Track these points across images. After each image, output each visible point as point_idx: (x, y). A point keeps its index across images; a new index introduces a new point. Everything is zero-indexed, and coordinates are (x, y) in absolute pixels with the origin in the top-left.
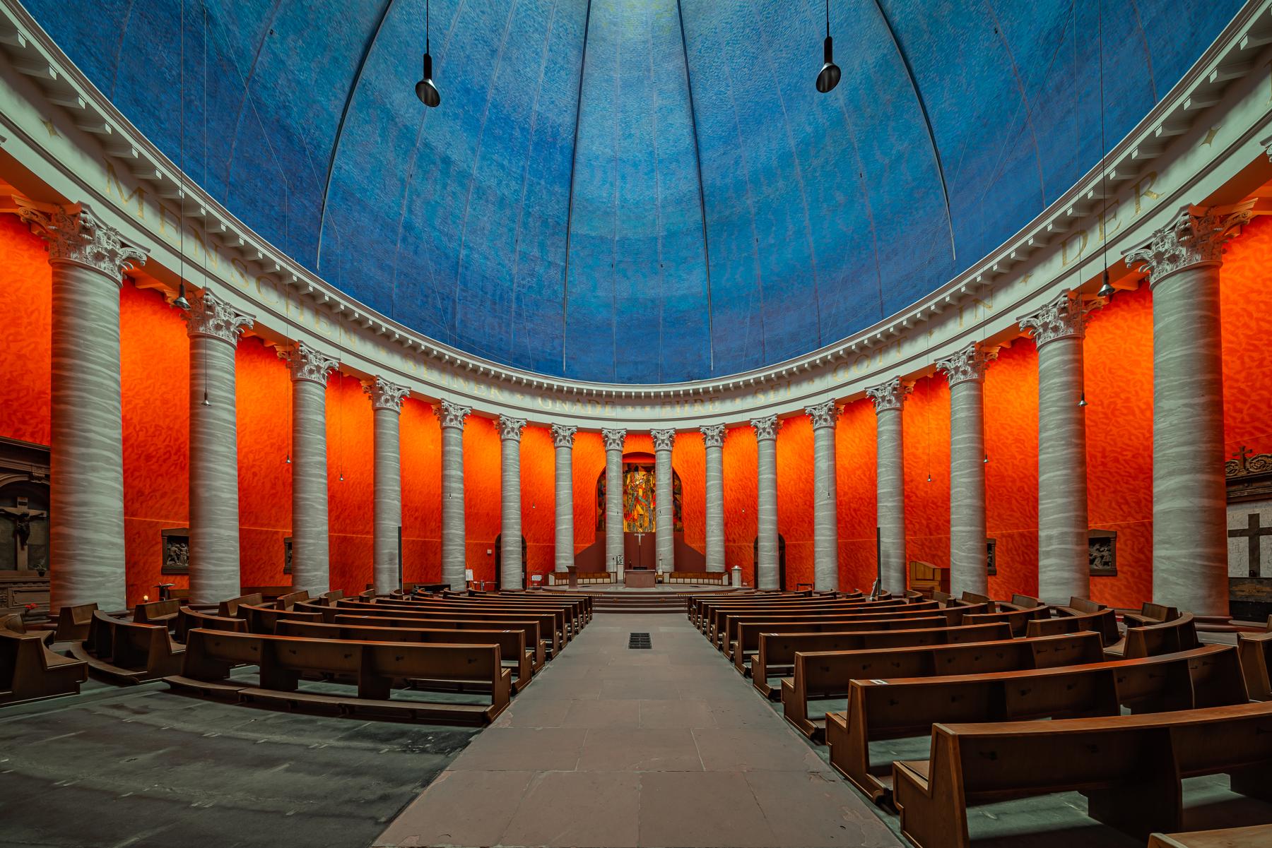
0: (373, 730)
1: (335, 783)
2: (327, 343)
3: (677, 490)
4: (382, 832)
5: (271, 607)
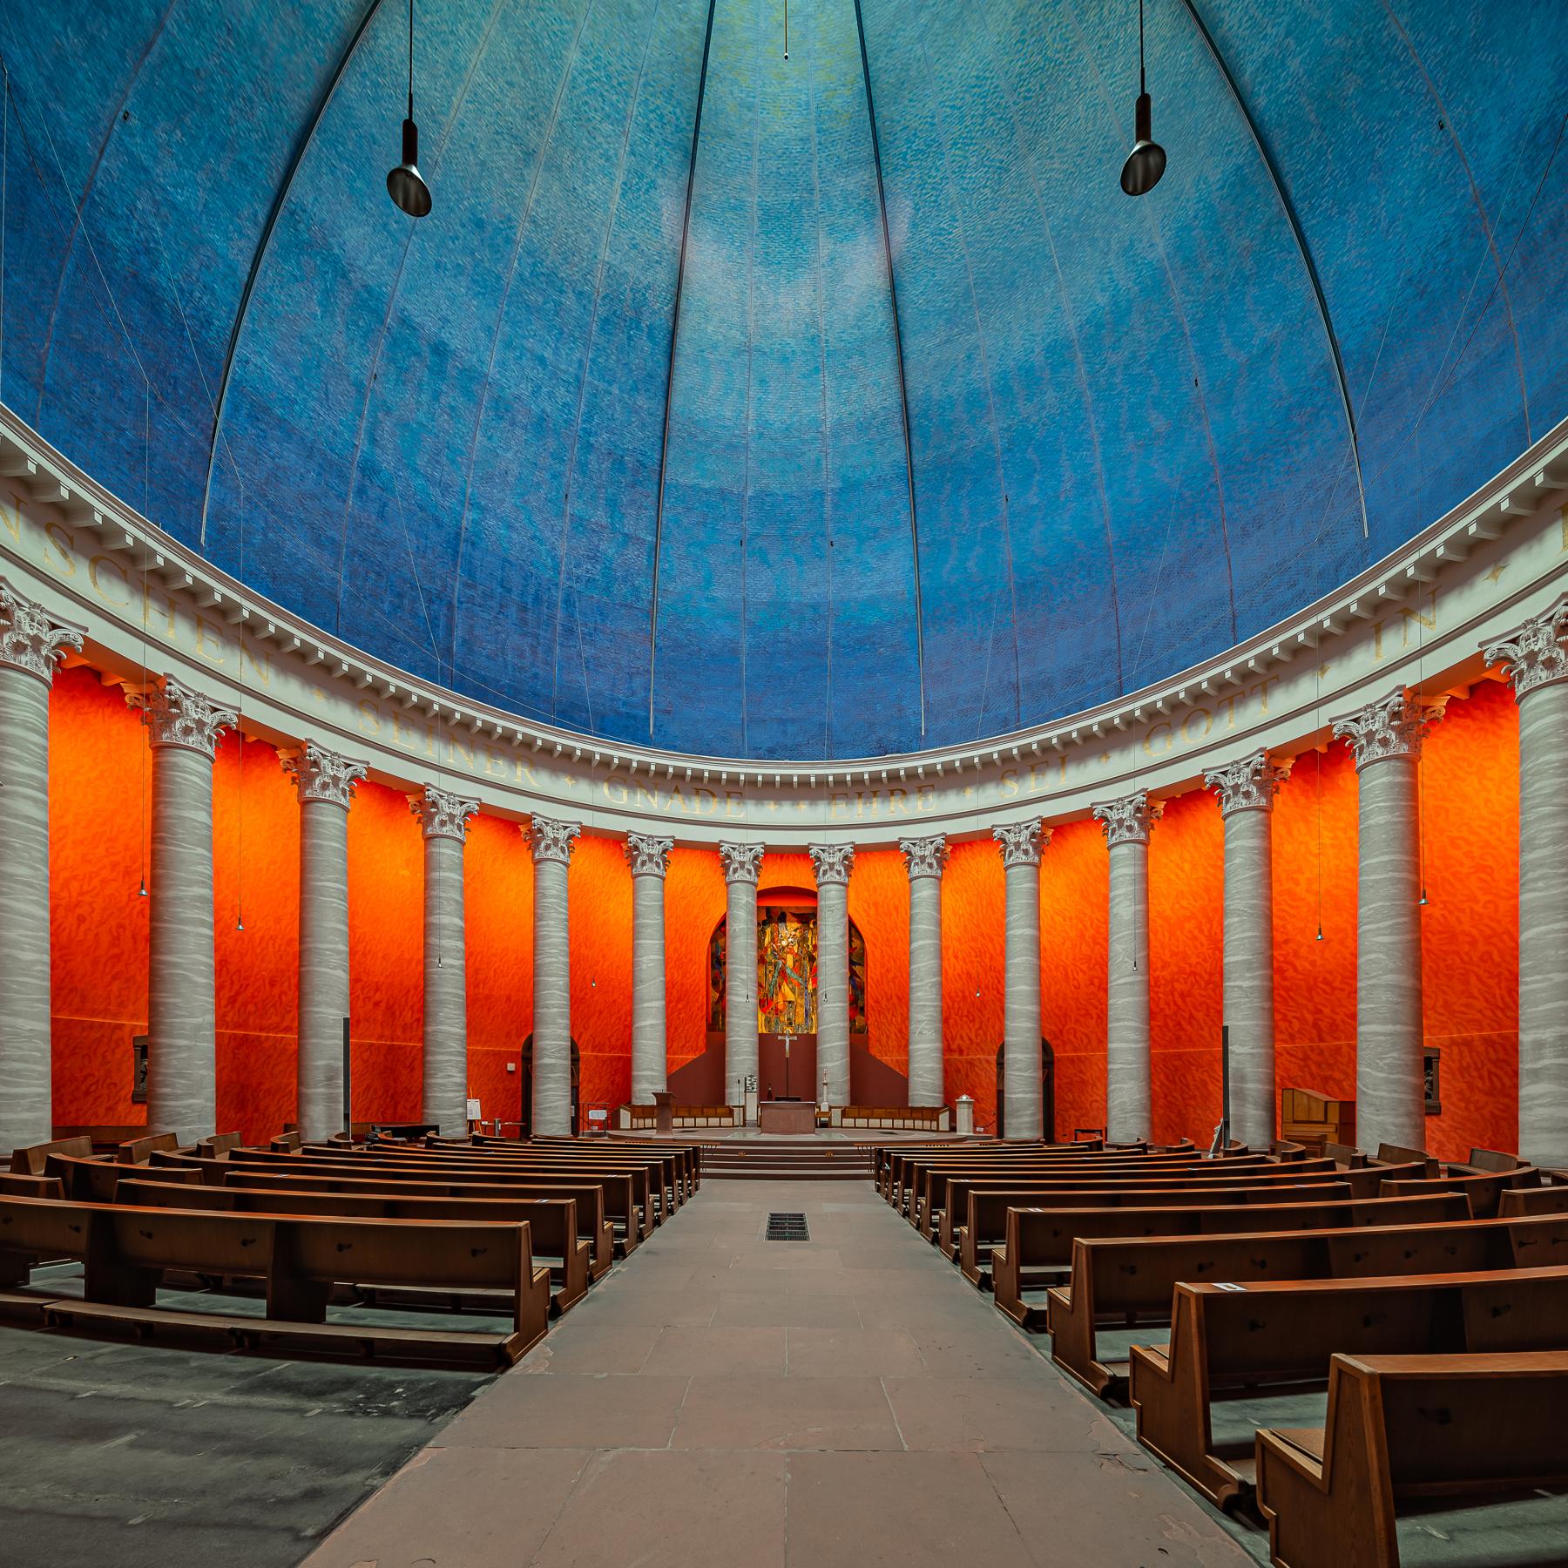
0: (293, 1377)
1: (222, 1468)
2: (215, 677)
3: (856, 958)
4: (308, 1553)
5: (110, 1160)
